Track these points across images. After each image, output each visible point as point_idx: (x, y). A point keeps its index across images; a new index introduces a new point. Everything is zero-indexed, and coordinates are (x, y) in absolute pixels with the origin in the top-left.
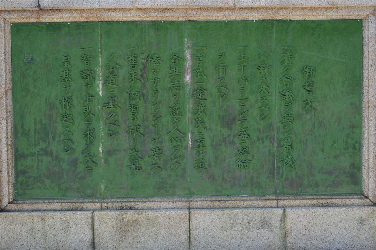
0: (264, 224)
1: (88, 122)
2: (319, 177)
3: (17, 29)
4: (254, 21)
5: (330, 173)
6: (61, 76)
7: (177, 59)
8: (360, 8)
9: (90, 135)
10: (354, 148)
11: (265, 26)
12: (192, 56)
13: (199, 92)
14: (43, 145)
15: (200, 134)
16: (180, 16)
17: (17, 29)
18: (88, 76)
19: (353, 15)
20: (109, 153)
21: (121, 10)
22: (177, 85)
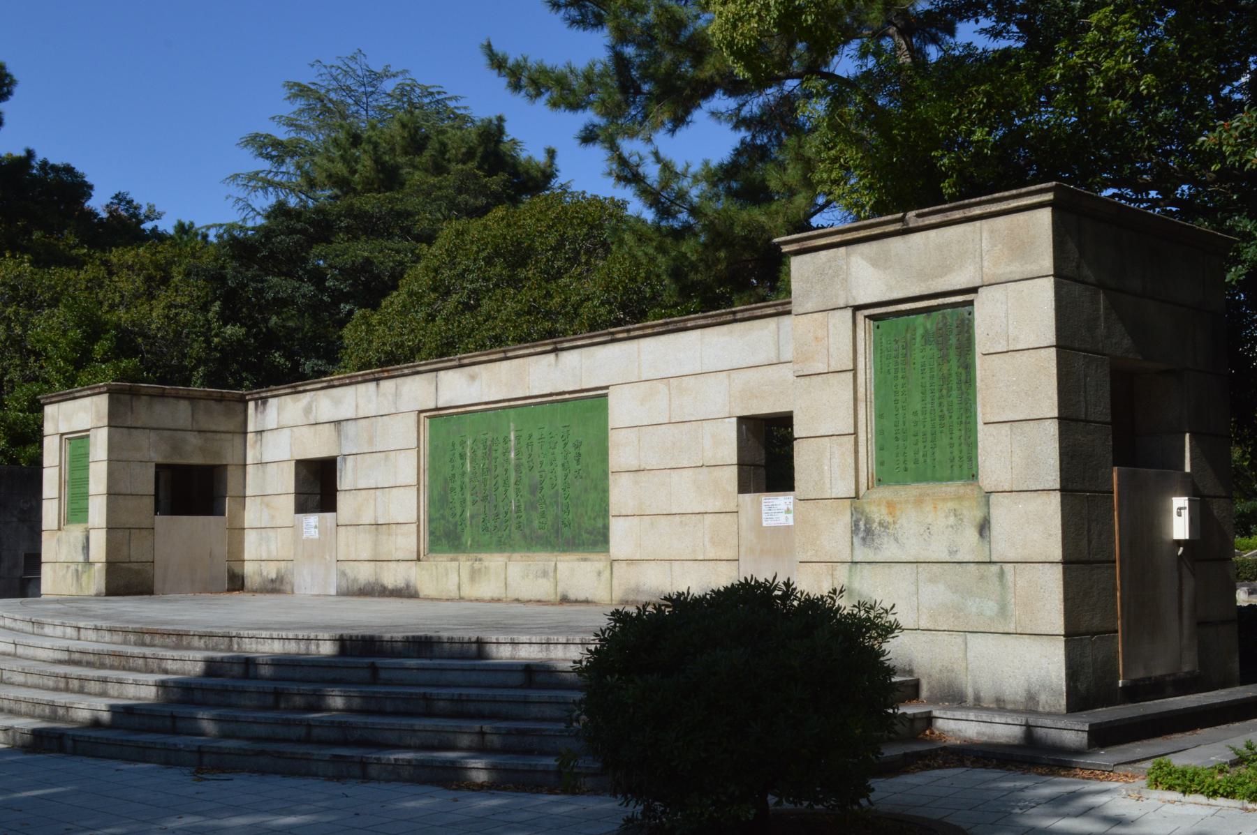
0: (545, 574)
7: (506, 440)
13: (518, 467)
20: (472, 517)
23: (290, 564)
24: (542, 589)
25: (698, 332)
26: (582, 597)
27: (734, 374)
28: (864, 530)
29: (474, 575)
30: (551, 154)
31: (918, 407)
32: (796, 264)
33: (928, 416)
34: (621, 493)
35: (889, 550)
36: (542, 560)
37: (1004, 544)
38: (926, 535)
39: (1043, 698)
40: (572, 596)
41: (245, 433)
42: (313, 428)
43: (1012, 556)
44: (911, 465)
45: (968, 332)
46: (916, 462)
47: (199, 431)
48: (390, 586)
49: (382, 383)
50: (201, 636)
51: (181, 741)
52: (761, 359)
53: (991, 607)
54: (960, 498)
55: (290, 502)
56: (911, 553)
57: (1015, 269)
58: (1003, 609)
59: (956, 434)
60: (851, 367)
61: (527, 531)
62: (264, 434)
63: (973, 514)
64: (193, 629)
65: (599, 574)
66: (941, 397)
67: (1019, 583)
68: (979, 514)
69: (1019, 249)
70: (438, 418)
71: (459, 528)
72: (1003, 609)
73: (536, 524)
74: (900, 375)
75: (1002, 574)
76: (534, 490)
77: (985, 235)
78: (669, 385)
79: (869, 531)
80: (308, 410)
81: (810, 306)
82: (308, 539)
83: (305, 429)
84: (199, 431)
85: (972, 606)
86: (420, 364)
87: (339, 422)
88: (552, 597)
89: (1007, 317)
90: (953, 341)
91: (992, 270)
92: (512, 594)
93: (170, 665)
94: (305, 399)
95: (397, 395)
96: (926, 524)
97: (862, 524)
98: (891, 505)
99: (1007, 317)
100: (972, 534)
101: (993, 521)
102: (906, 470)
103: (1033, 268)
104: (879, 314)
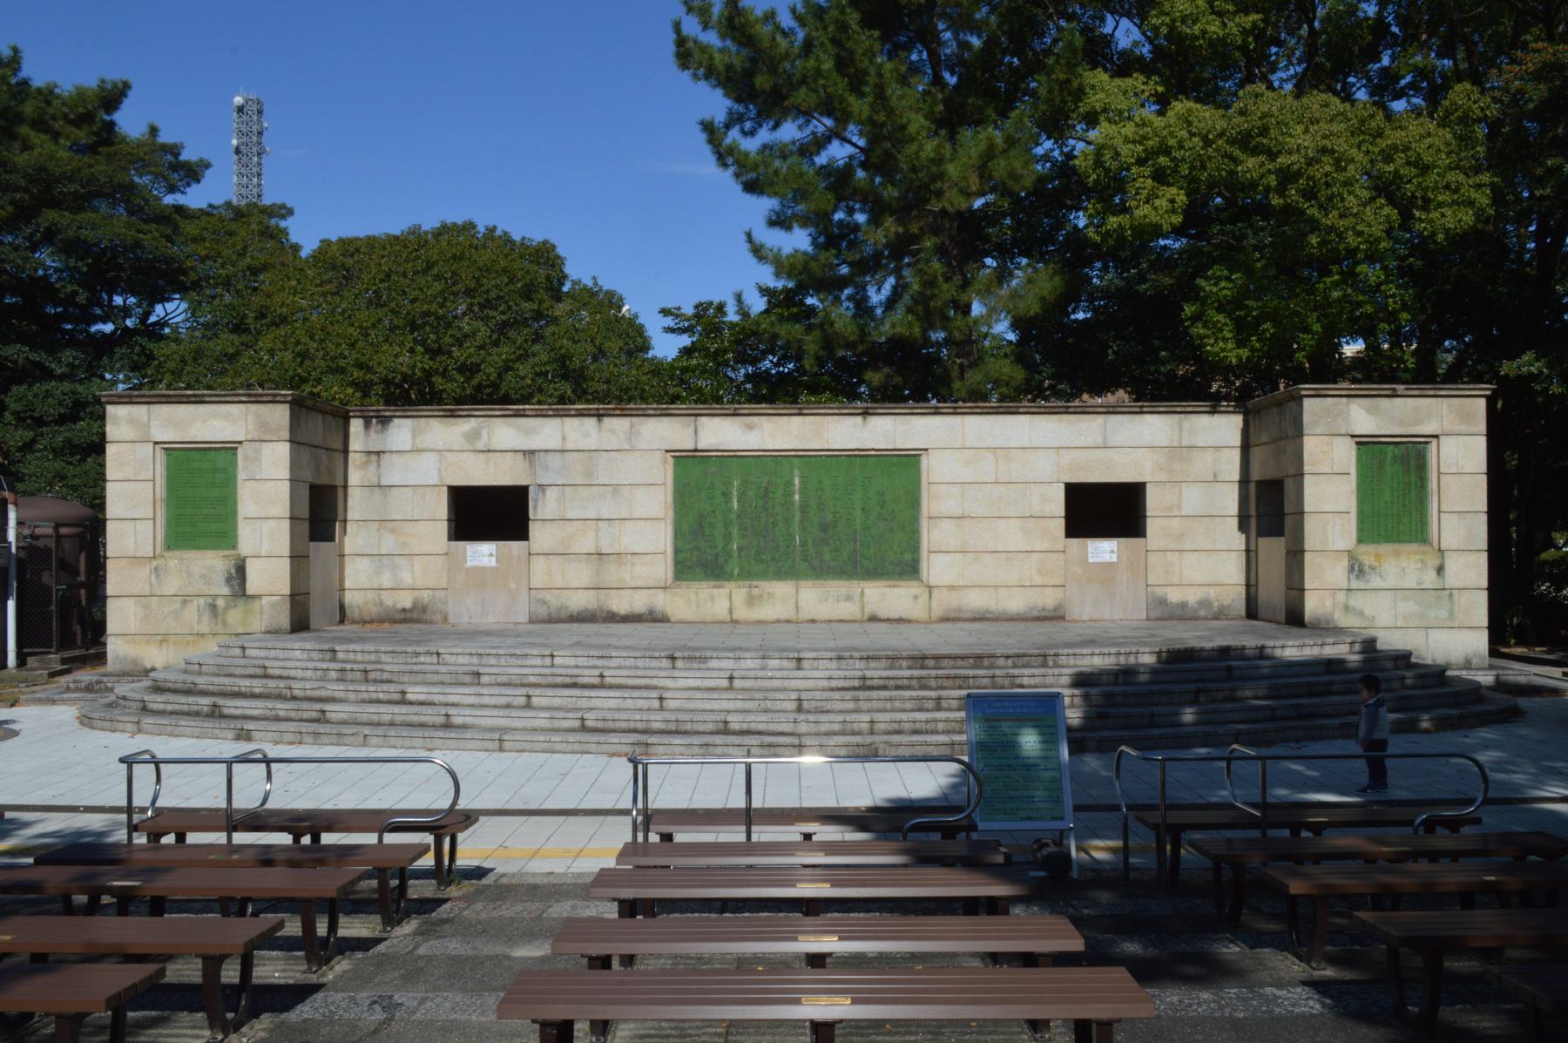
0: (849, 598)
7: (789, 483)
9: (728, 537)
13: (804, 509)
18: (726, 495)
20: (740, 549)
22: (788, 502)
23: (442, 594)
24: (848, 610)
25: (1028, 417)
26: (895, 615)
27: (1062, 452)
28: (1357, 569)
29: (751, 601)
32: (1306, 402)
34: (933, 535)
35: (1376, 582)
36: (855, 587)
37: (1451, 579)
39: (1475, 661)
40: (882, 615)
41: (346, 451)
42: (482, 456)
43: (1457, 585)
48: (622, 612)
49: (606, 420)
50: (1007, 657)
51: (1481, 708)
52: (1089, 442)
53: (1443, 613)
54: (1425, 553)
56: (1391, 583)
57: (1463, 428)
58: (1451, 614)
61: (816, 563)
62: (385, 458)
64: (999, 652)
65: (916, 597)
68: (1437, 562)
70: (687, 461)
71: (721, 560)
72: (1451, 614)
73: (827, 556)
75: (1451, 596)
76: (824, 528)
79: (1361, 571)
80: (473, 436)
81: (1318, 431)
82: (476, 568)
83: (471, 455)
86: (678, 407)
87: (532, 452)
88: (859, 617)
90: (1413, 462)
91: (1447, 426)
92: (804, 616)
93: (1026, 681)
94: (465, 426)
95: (631, 434)
96: (1401, 568)
98: (1378, 556)
100: (1432, 574)
103: (1474, 429)
104: (1364, 444)
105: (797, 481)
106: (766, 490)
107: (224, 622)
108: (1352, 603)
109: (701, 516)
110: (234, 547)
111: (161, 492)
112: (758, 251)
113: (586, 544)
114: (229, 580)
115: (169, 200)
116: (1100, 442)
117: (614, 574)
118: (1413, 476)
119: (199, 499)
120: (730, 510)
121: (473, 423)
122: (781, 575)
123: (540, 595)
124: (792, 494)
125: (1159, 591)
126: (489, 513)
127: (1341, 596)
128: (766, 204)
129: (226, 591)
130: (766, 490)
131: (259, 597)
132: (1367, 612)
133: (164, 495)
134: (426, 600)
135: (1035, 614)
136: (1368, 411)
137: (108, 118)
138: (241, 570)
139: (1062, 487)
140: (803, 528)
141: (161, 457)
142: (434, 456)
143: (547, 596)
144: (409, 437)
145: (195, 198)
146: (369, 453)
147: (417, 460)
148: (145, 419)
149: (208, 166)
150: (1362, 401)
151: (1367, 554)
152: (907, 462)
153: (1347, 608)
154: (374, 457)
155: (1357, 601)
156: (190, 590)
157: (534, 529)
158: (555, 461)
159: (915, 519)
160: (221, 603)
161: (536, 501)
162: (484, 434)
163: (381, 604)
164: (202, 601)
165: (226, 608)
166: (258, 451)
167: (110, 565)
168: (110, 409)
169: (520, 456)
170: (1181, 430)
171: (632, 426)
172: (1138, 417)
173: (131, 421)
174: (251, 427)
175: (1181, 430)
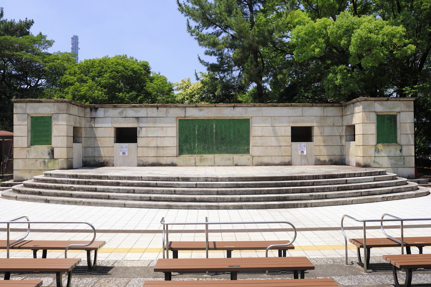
0: (229, 159)
1: (194, 139)
2: (241, 151)
3: (180, 120)
4: (264, 15)
5: (243, 150)
6: (3, 8)
7: (212, 126)
8: (249, 117)
10: (248, 145)
11: (230, 120)
12: (215, 126)
13: (216, 133)
14: (185, 144)
15: (217, 142)
16: (213, 118)
17: (180, 120)
18: (194, 130)
19: (247, 118)
21: (201, 117)
30: (75, 40)
31: (386, 130)
33: (388, 132)
37: (404, 153)
38: (390, 152)
43: (406, 155)
44: (384, 140)
45: (193, 184)
46: (385, 139)
47: (79, 116)
55: (113, 139)
57: (407, 110)
58: (404, 164)
59: (393, 135)
60: (186, 116)
63: (399, 148)
65: (249, 159)
66: (390, 129)
67: (407, 159)
68: (400, 148)
69: (408, 107)
72: (404, 164)
74: (382, 124)
75: (404, 158)
77: (402, 103)
78: (289, 118)
79: (378, 151)
84: (79, 116)
85: (399, 163)
87: (138, 118)
89: (406, 117)
94: (119, 110)
95: (167, 112)
97: (377, 150)
99: (406, 117)
100: (399, 152)
101: (403, 150)
102: (383, 140)
105: (214, 126)
106: (205, 128)
107: (48, 166)
108: (376, 160)
109: (187, 136)
110: (51, 144)
111: (30, 129)
112: (202, 62)
113: (153, 144)
114: (49, 154)
115: (43, 51)
116: (301, 114)
117: (161, 152)
118: (393, 124)
119: (41, 131)
120: (195, 134)
121: (121, 109)
122: (210, 153)
123: (140, 159)
124: (213, 129)
125: (318, 157)
126: (126, 136)
127: (373, 158)
128: (204, 49)
129: (48, 157)
130: (205, 128)
131: (58, 159)
132: (380, 163)
133: (30, 129)
134: (108, 160)
135: (283, 164)
136: (380, 105)
137: (28, 30)
138: (52, 151)
139: (290, 127)
140: (216, 139)
141: (30, 119)
142: (110, 119)
143: (142, 159)
144: (103, 113)
145: (51, 50)
146: (92, 118)
147: (109, 120)
148: (25, 107)
149: (54, 41)
150: (378, 102)
151: (380, 146)
152: (246, 122)
153: (374, 162)
154: (93, 119)
155: (378, 160)
156: (38, 157)
157: (139, 140)
158: (144, 120)
159: (248, 137)
160: (46, 160)
161: (139, 131)
162: (124, 112)
163: (95, 161)
164: (41, 160)
165: (48, 162)
166: (58, 116)
167: (15, 150)
168: (15, 104)
169: (135, 118)
170: (324, 111)
171: (167, 110)
172: (312, 108)
173: (21, 108)
174: (55, 109)
175: (324, 111)
